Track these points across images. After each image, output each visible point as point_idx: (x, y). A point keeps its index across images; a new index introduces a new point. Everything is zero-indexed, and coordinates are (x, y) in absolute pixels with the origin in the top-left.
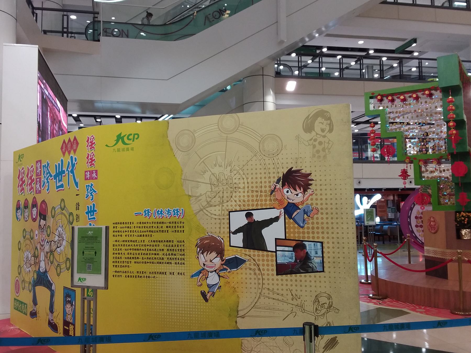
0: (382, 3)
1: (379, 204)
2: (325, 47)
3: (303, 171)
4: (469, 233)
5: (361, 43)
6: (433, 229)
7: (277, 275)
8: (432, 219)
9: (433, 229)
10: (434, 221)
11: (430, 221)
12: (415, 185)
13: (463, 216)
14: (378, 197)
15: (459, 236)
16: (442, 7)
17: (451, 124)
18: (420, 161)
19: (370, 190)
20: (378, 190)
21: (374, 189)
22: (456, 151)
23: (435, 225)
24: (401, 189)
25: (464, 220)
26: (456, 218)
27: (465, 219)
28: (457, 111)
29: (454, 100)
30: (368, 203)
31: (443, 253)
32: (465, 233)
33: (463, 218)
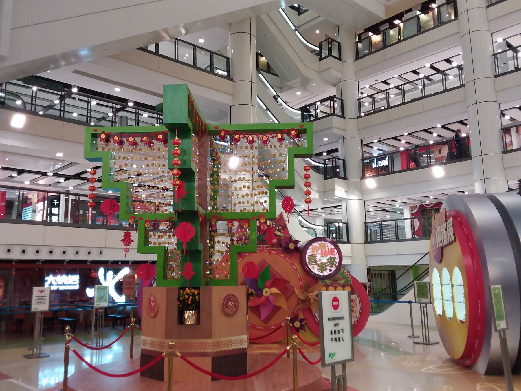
0: (141, 49)
1: (126, 280)
2: (75, 86)
3: (291, 284)
4: (193, 316)
5: (117, 91)
6: (152, 312)
7: (142, 350)
8: (152, 299)
9: (152, 312)
10: (154, 301)
11: (150, 301)
12: (140, 251)
13: (187, 294)
14: (125, 271)
15: (181, 320)
16: (205, 70)
17: (175, 172)
18: (146, 221)
19: (115, 263)
20: (125, 263)
21: (120, 261)
22: (183, 208)
23: (155, 306)
24: (150, 262)
25: (188, 299)
26: (179, 297)
27: (189, 298)
28: (185, 158)
29: (180, 142)
30: (114, 277)
31: (161, 345)
32: (188, 316)
33: (186, 297)
